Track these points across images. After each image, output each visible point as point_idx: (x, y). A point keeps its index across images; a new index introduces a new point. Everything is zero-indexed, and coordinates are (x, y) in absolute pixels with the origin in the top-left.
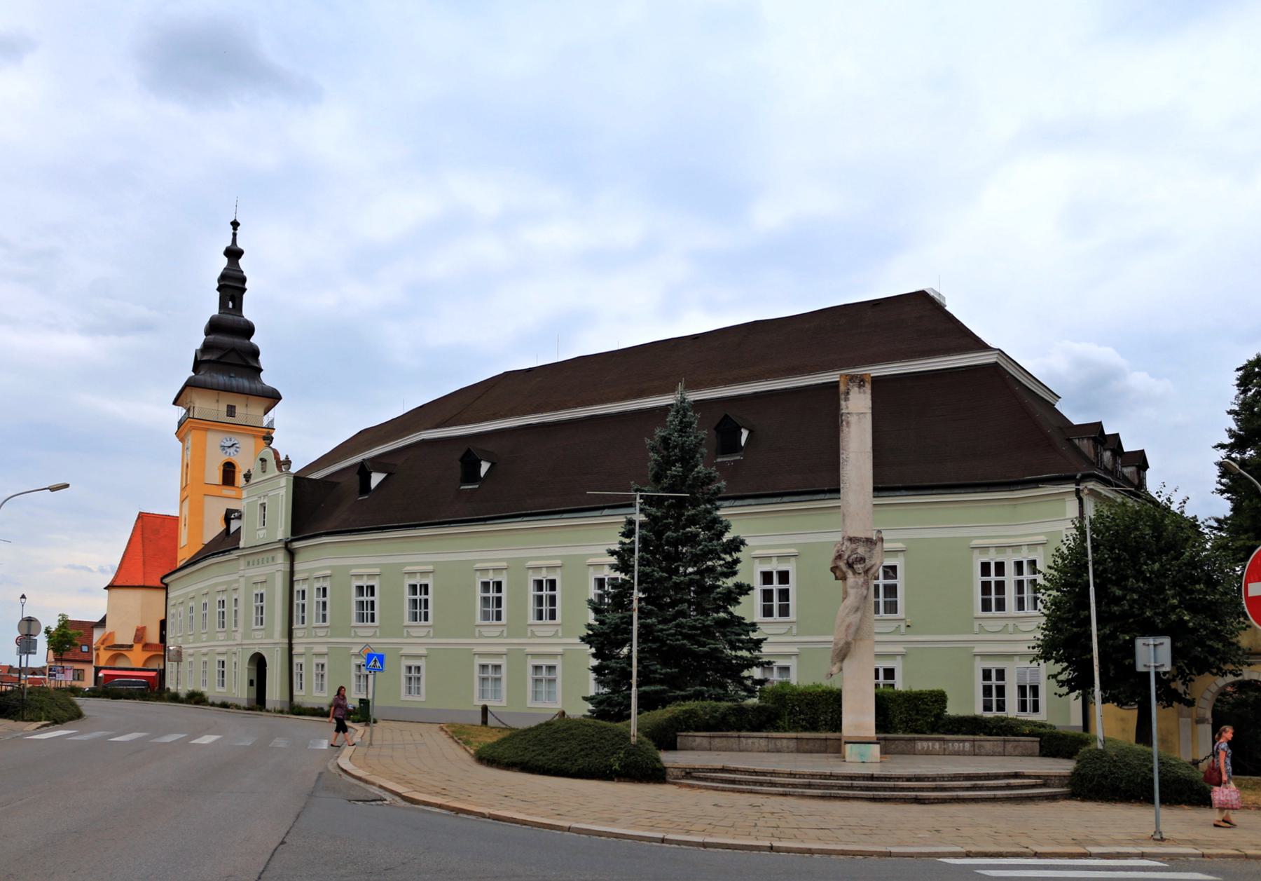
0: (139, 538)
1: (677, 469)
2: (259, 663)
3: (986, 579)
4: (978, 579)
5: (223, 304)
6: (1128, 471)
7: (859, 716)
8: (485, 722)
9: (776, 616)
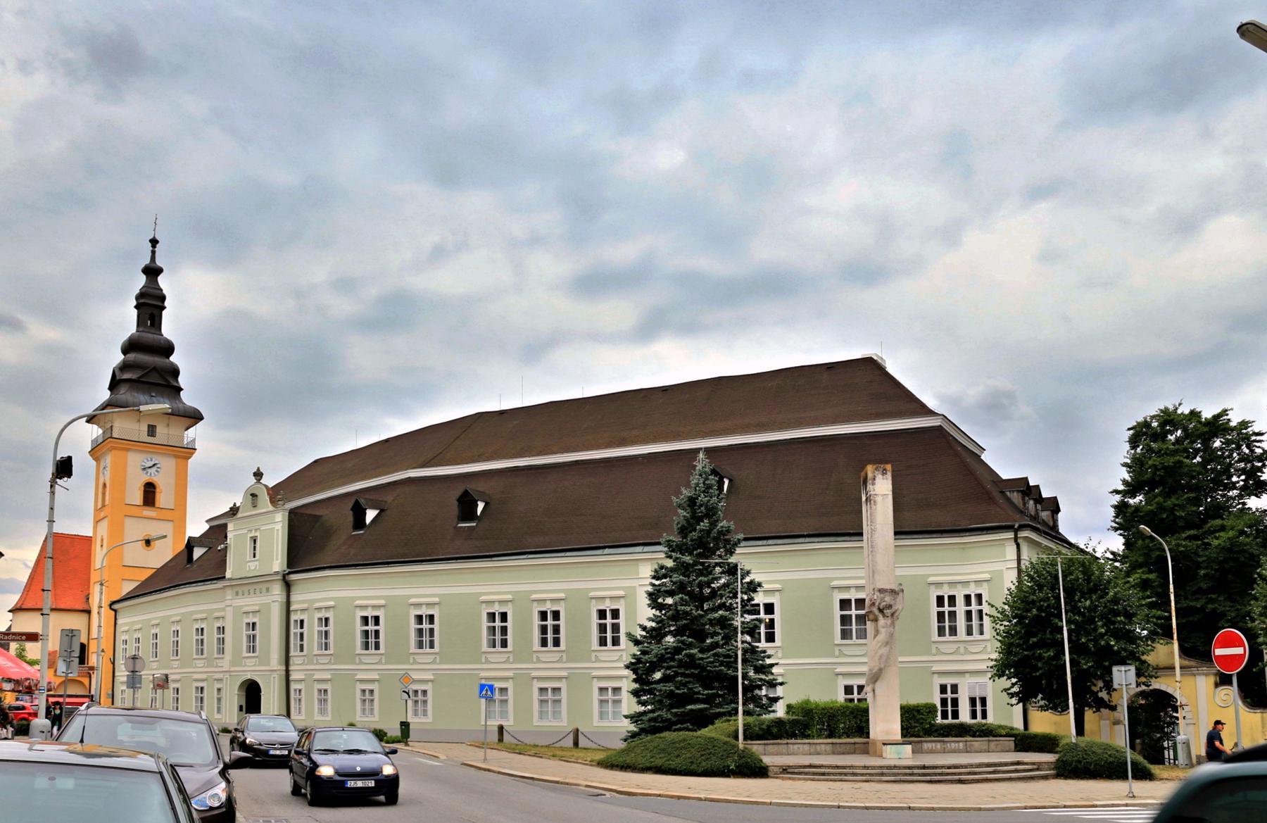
1: (705, 524)
3: (941, 609)
4: (935, 609)
5: (140, 322)
6: (1045, 515)
7: (885, 723)
8: (501, 740)
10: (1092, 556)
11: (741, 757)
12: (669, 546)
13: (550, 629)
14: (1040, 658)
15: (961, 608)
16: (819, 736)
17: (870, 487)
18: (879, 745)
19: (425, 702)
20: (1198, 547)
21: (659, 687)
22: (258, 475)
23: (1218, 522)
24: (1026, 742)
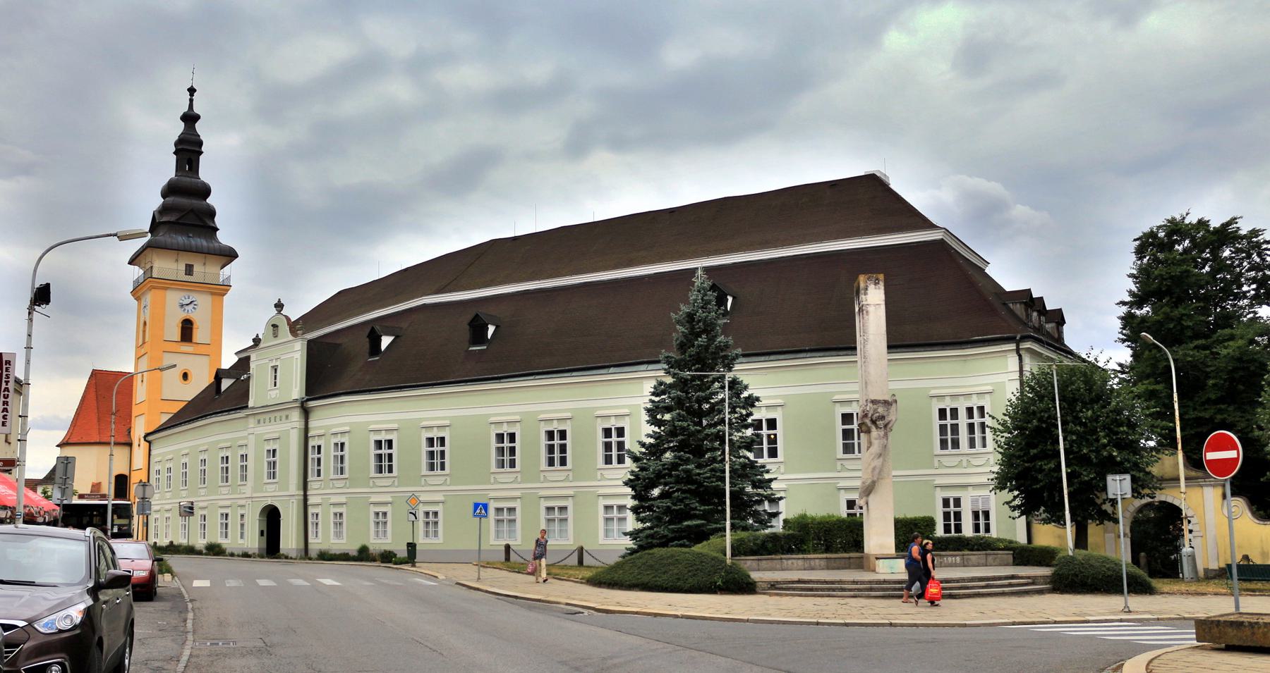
0: (92, 395)
1: (703, 340)
2: (272, 517)
3: (943, 422)
4: (937, 423)
7: (879, 537)
8: (508, 559)
9: (557, 466)
10: (1094, 365)
11: (728, 573)
12: (668, 363)
13: (557, 447)
14: (1041, 470)
15: (963, 421)
16: (815, 551)
17: (862, 297)
18: (872, 559)
19: (436, 523)
20: (1206, 357)
21: (657, 503)
22: (279, 306)
23: (1228, 331)
24: (1025, 555)
